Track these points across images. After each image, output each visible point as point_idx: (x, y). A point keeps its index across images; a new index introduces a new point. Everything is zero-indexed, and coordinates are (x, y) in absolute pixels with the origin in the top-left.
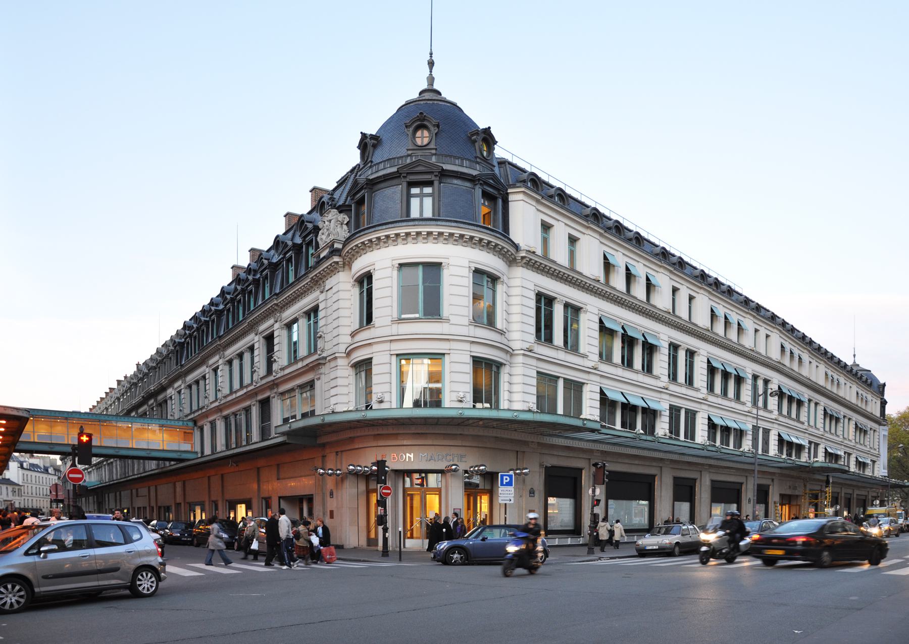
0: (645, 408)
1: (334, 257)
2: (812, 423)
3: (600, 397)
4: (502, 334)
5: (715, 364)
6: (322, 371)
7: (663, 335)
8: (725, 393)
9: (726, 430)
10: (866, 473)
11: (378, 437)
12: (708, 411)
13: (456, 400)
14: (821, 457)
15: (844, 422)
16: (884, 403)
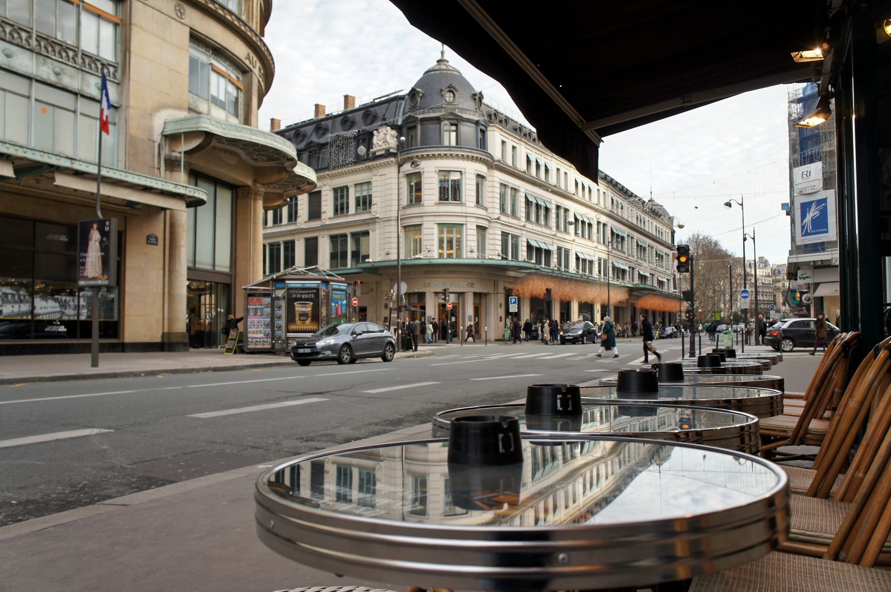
2: (630, 253)
5: (531, 199)
7: (553, 200)
9: (539, 250)
10: (664, 291)
11: (427, 272)
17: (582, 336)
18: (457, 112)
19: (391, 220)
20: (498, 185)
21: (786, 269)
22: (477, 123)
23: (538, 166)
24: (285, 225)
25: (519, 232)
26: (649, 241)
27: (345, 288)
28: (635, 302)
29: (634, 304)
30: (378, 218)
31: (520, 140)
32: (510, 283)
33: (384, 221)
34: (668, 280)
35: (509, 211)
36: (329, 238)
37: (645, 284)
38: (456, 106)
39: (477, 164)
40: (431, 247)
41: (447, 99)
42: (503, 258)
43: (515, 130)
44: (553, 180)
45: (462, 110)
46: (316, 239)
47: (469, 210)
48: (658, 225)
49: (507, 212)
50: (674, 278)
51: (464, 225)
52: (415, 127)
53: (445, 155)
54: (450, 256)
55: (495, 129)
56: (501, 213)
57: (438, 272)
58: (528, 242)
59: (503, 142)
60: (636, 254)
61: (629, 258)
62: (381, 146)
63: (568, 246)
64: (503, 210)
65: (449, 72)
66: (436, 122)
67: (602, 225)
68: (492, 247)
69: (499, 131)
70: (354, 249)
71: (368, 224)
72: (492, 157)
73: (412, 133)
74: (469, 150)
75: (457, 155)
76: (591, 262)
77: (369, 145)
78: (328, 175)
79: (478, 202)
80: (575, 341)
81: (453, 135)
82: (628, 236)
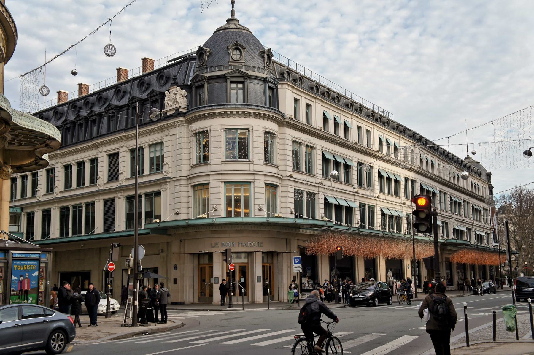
0: (337, 205)
1: (180, 117)
2: (443, 208)
3: (324, 202)
4: (277, 168)
5: (328, 156)
6: (168, 186)
7: (354, 157)
8: (389, 192)
9: (339, 207)
10: (483, 245)
12: (380, 205)
13: (258, 209)
14: (451, 235)
15: (464, 205)
16: (491, 188)
17: (373, 297)
18: (243, 69)
19: (180, 180)
20: (290, 143)
21: (75, 270)
22: (265, 80)
23: (336, 124)
24: (87, 187)
25: (317, 189)
26: (464, 197)
27: (37, 256)
28: (451, 256)
29: (449, 258)
30: (169, 178)
31: (315, 98)
32: (304, 241)
33: (174, 181)
34: (488, 234)
35: (303, 168)
36: (125, 199)
37: (461, 239)
38: (243, 64)
39: (266, 121)
40: (218, 206)
41: (234, 57)
42: (296, 217)
43: (312, 88)
44: (353, 137)
45: (249, 67)
46: (113, 200)
47: (257, 168)
48: (474, 181)
49: (301, 170)
50: (494, 232)
51: (252, 184)
52: (202, 86)
53: (231, 112)
54: (238, 214)
55: (286, 86)
56: (294, 171)
57: (224, 232)
58: (326, 199)
59: (296, 100)
60: (449, 209)
61: (442, 213)
62: (171, 106)
63: (372, 202)
64: (296, 167)
65: (237, 30)
66: (222, 80)
67: (410, 182)
68: (284, 205)
69: (291, 89)
70: (149, 210)
71: (160, 184)
72: (283, 115)
73: (200, 92)
74: (256, 108)
75: (244, 112)
76: (399, 218)
77: (162, 106)
78: (124, 136)
79: (266, 159)
80: (367, 303)
81: (240, 92)
82: (440, 192)
